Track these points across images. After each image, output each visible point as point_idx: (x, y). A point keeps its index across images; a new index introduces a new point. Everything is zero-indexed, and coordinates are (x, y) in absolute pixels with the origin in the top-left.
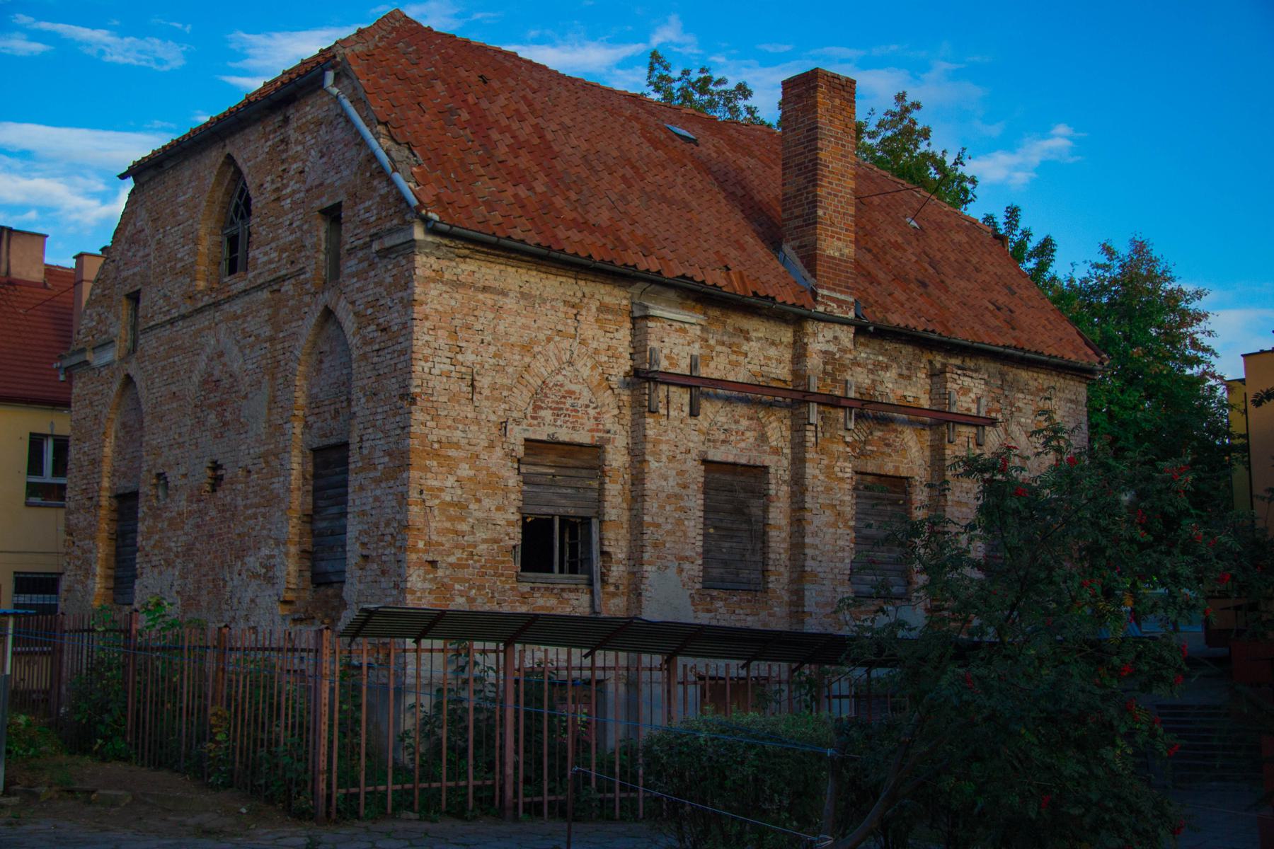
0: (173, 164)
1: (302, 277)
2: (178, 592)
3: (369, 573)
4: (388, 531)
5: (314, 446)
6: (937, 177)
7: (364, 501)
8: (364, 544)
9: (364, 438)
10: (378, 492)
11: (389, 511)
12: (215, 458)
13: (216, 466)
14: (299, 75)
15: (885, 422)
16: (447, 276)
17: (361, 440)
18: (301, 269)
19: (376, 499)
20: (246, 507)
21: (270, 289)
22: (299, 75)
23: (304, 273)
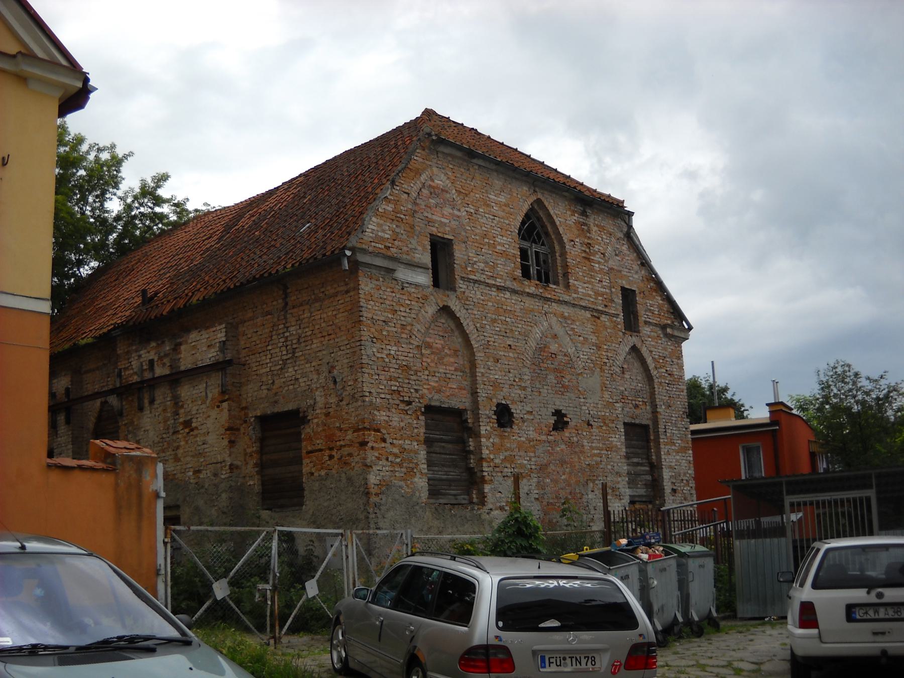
0: (483, 164)
1: (615, 319)
2: (537, 499)
3: (678, 498)
4: (685, 478)
5: (626, 421)
6: (708, 393)
7: (671, 460)
8: (673, 483)
9: (667, 427)
10: (678, 457)
11: (684, 468)
12: (557, 407)
13: (558, 413)
14: (617, 205)
15: (732, 589)
16: (421, 289)
17: (665, 428)
18: (616, 314)
19: (677, 461)
20: (592, 448)
21: (591, 313)
22: (617, 205)
23: (617, 318)
